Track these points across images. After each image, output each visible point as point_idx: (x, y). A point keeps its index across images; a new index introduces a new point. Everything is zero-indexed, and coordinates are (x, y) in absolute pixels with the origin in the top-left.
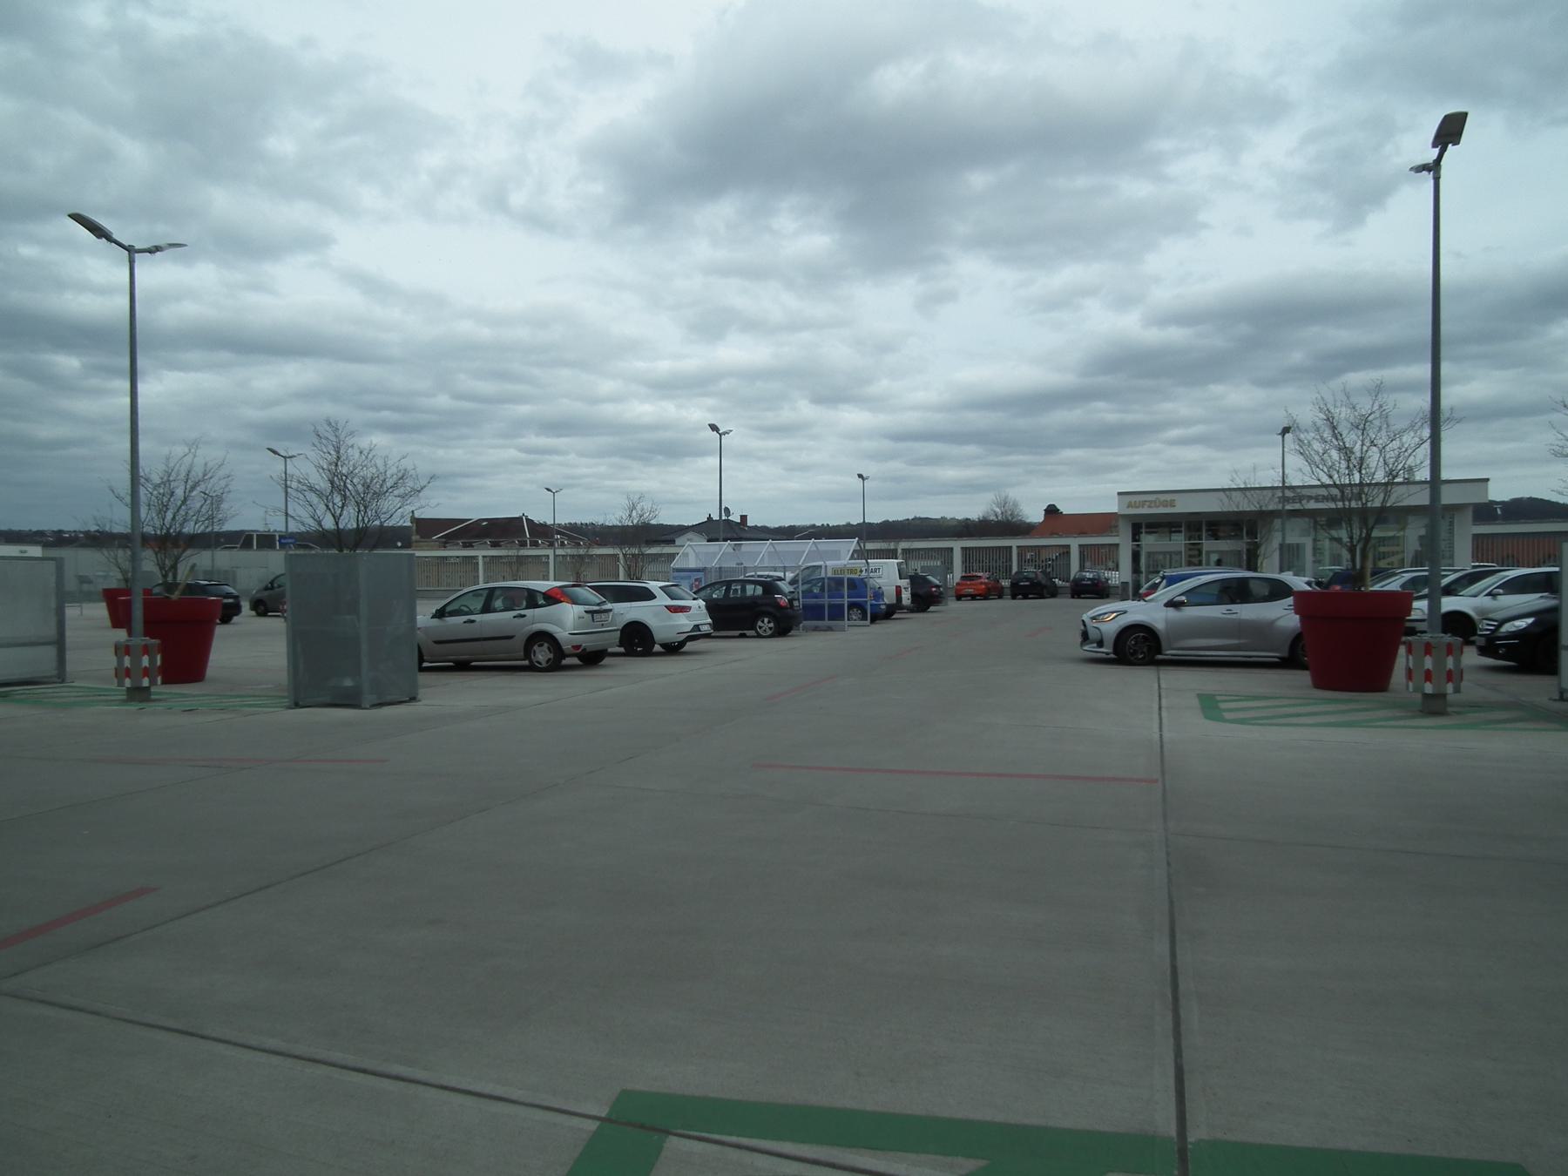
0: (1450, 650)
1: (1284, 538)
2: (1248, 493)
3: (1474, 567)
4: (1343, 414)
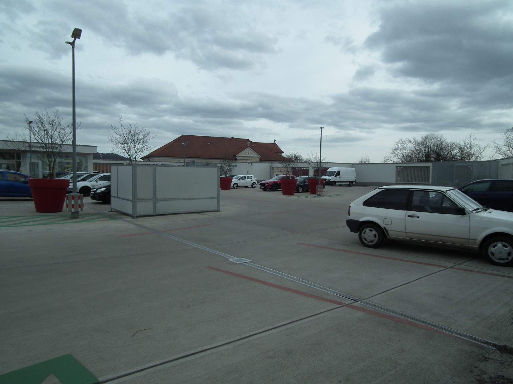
0: (80, 198)
1: (31, 160)
2: (14, 143)
3: (93, 173)
4: (45, 119)
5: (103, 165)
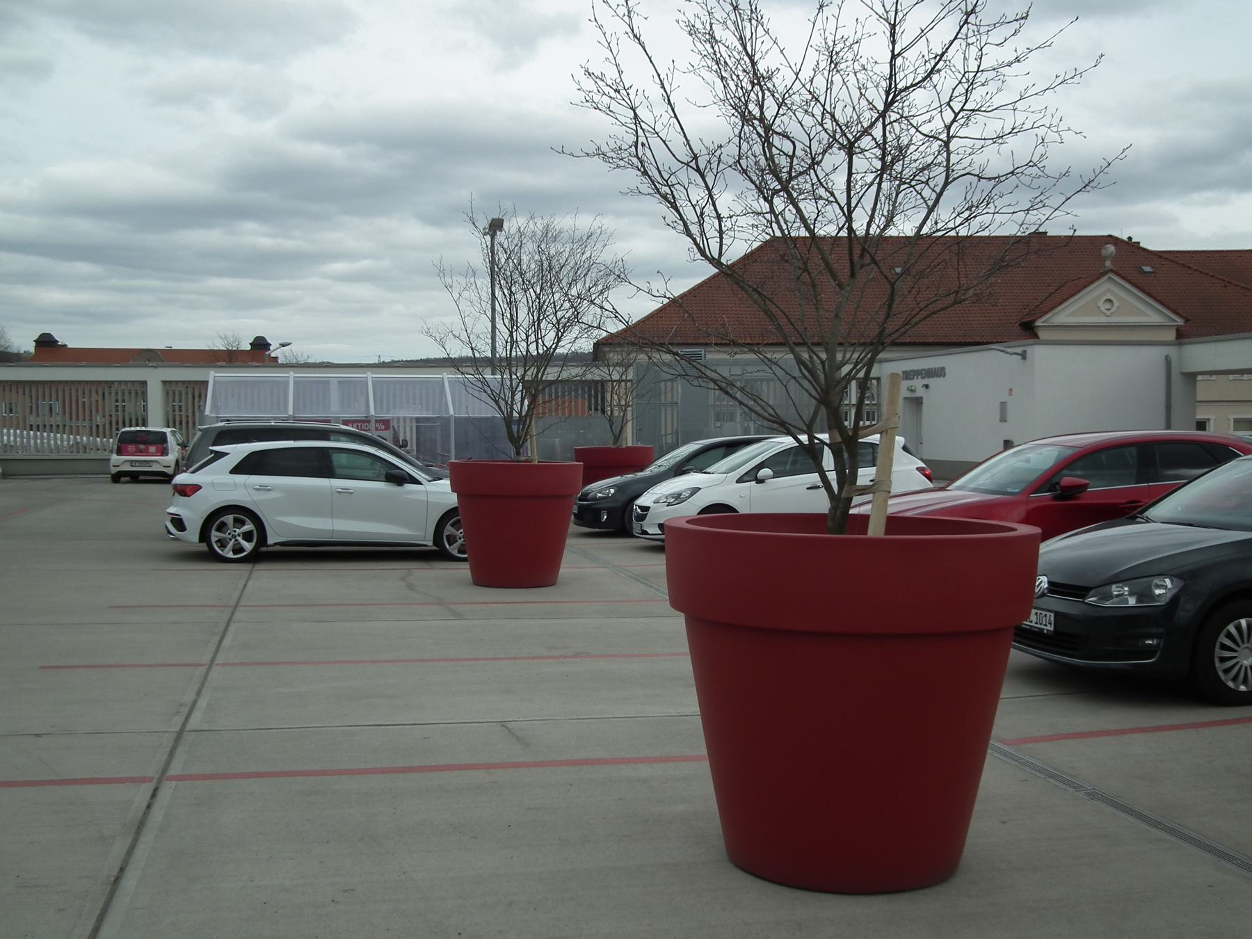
5: (669, 413)
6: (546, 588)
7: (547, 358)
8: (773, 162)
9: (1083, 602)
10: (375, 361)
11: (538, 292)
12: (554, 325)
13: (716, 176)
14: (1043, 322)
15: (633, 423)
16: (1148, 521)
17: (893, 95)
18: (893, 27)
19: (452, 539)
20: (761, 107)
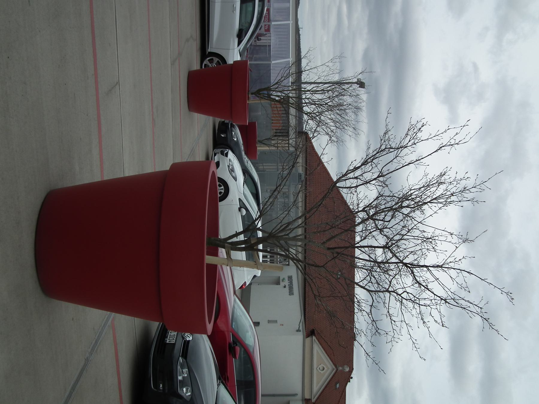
6: (188, 108)
7: (300, 109)
8: (382, 212)
9: (180, 356)
10: (300, 26)
11: (328, 104)
12: (313, 111)
13: (374, 184)
14: (314, 339)
15: (268, 150)
16: (218, 385)
17: (411, 267)
18: (441, 267)
19: (211, 61)
20: (407, 207)
